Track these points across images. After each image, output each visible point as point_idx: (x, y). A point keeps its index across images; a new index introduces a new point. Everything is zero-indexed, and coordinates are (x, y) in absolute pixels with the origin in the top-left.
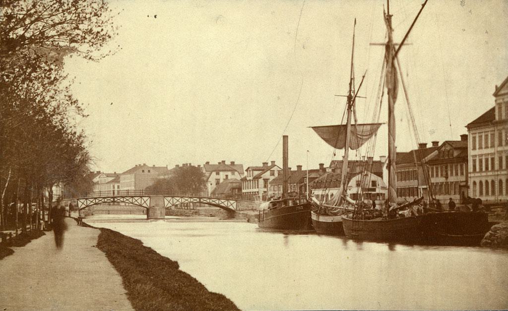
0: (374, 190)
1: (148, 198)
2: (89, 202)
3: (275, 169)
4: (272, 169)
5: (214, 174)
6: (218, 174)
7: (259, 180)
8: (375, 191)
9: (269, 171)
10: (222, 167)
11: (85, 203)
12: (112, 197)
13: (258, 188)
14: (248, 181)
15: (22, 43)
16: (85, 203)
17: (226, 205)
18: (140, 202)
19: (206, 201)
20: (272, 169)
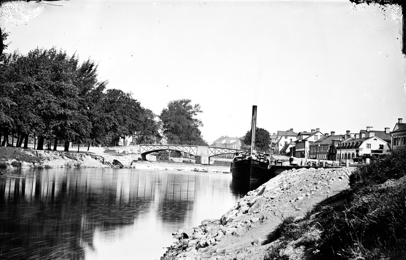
0: (381, 152)
1: (152, 146)
2: (217, 151)
3: (318, 134)
4: (315, 135)
5: (283, 137)
6: (286, 137)
7: (306, 142)
8: (382, 153)
9: (314, 136)
10: (314, 133)
11: (214, 152)
12: (235, 150)
13: (305, 148)
14: (299, 143)
15: (341, 240)
16: (214, 152)
17: (175, 149)
18: (228, 152)
19: (232, 151)
20: (315, 135)
